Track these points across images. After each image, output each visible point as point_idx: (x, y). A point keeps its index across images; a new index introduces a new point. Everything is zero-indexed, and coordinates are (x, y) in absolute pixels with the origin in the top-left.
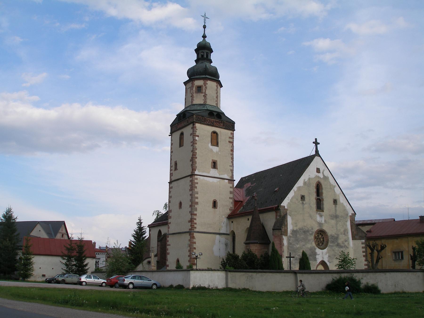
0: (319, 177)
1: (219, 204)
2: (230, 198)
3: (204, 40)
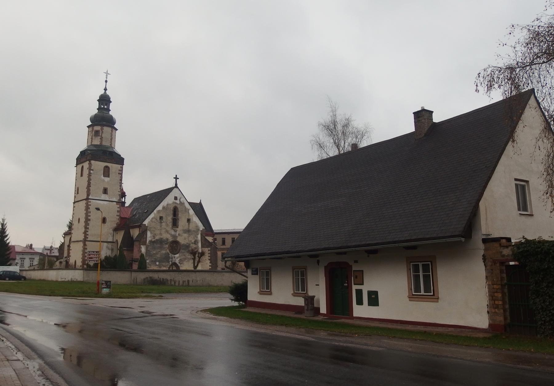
0: (176, 203)
1: (108, 220)
2: (117, 216)
3: (105, 92)
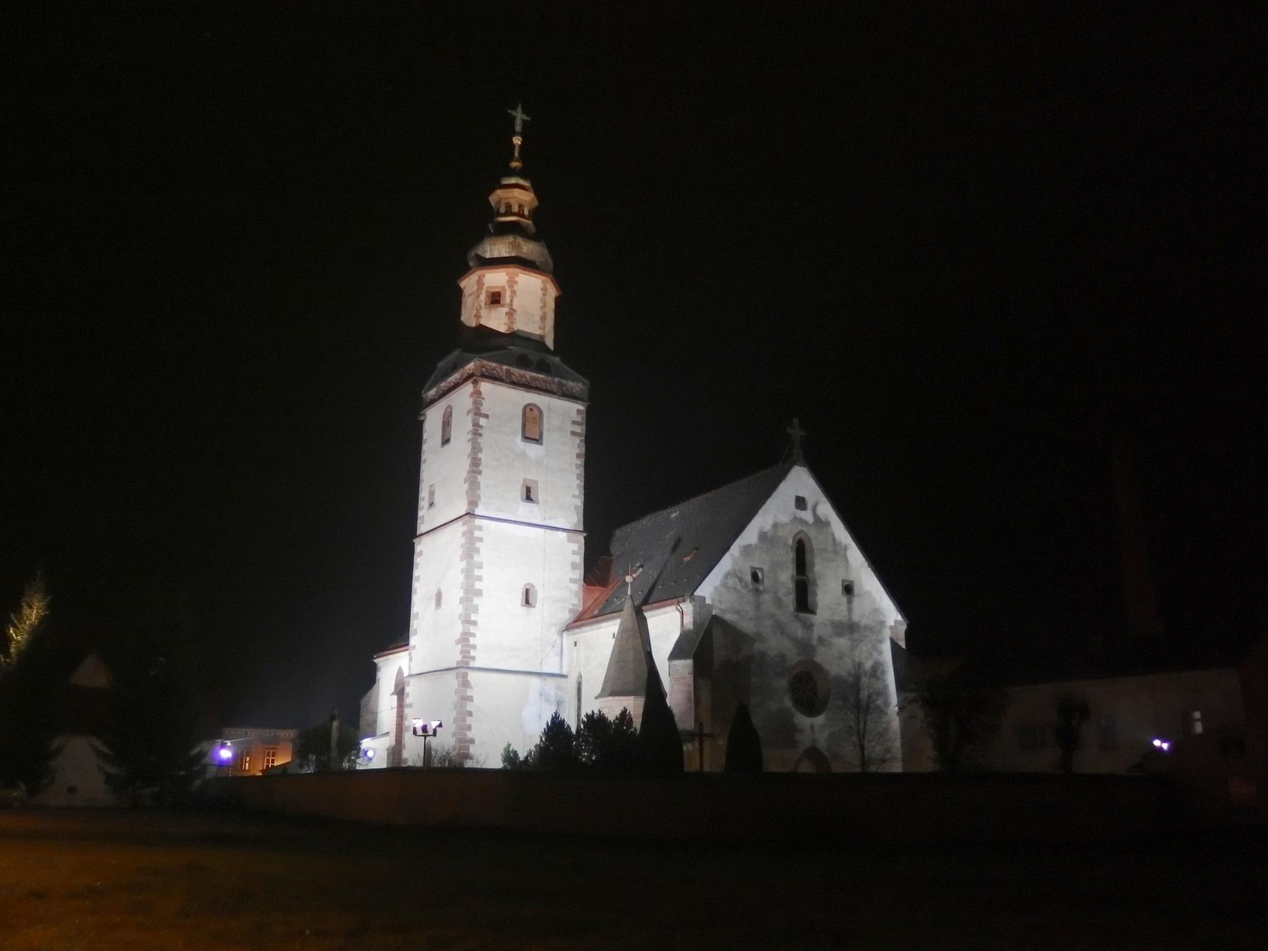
0: (802, 521)
1: (540, 595)
